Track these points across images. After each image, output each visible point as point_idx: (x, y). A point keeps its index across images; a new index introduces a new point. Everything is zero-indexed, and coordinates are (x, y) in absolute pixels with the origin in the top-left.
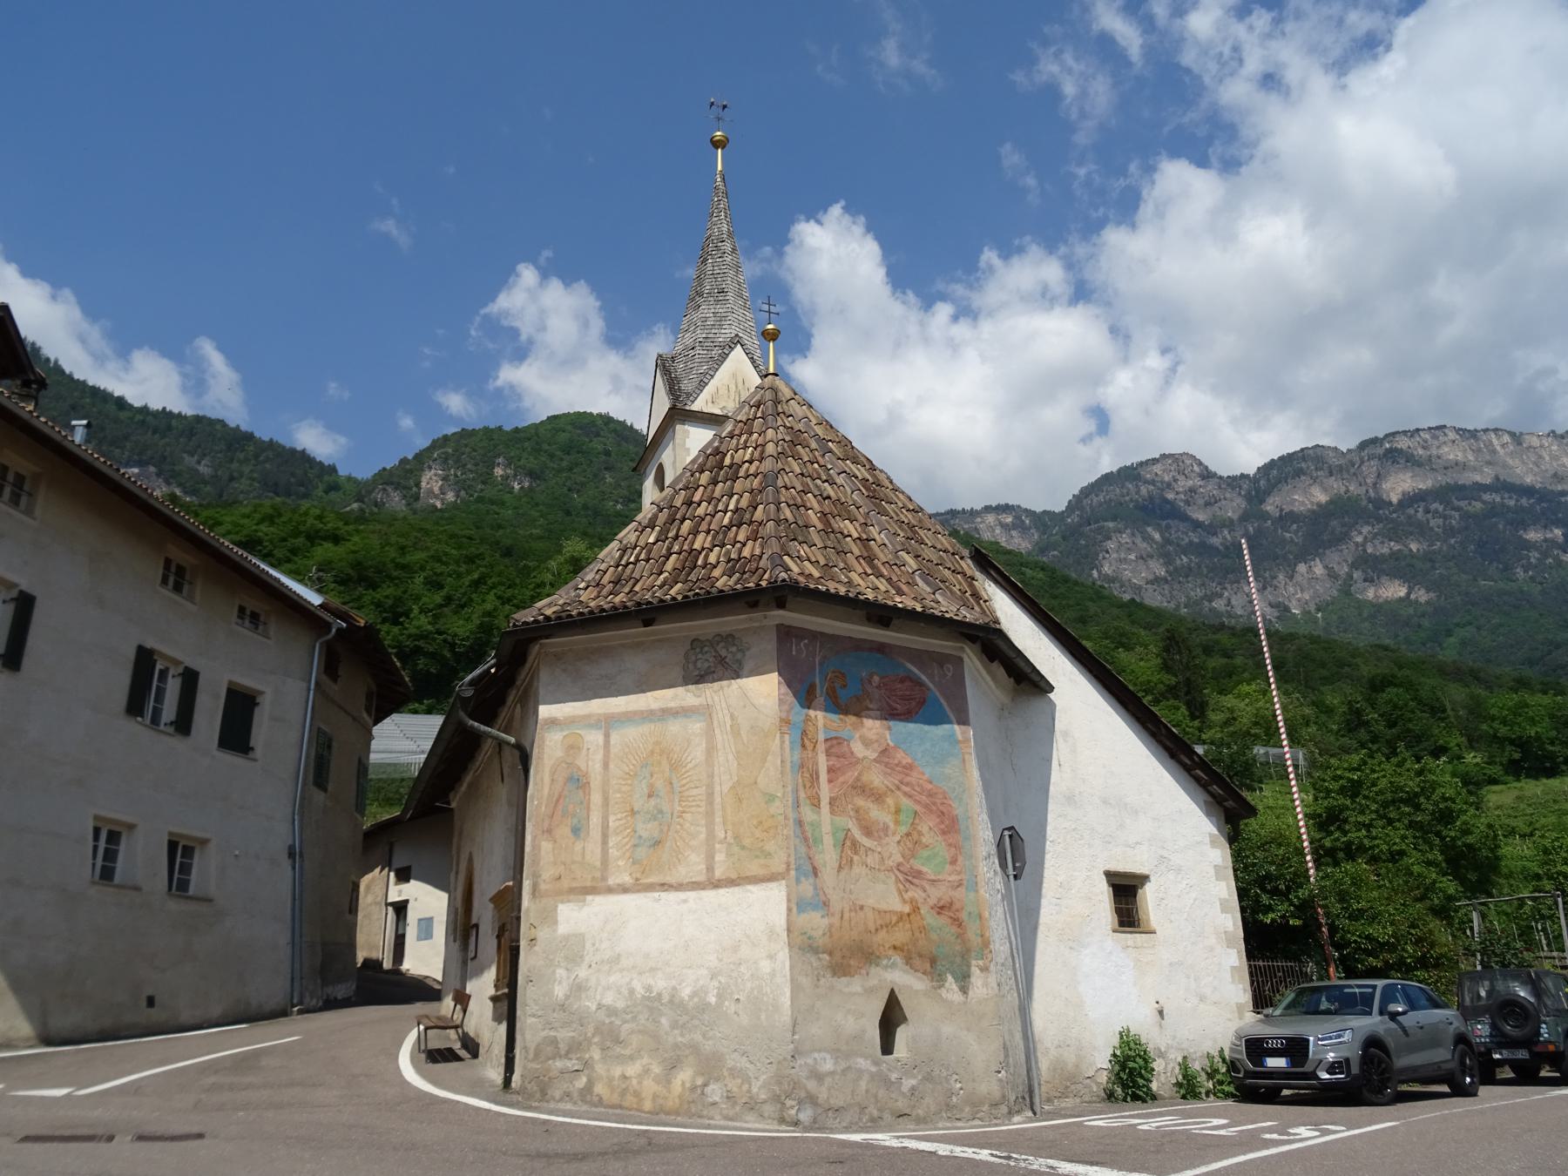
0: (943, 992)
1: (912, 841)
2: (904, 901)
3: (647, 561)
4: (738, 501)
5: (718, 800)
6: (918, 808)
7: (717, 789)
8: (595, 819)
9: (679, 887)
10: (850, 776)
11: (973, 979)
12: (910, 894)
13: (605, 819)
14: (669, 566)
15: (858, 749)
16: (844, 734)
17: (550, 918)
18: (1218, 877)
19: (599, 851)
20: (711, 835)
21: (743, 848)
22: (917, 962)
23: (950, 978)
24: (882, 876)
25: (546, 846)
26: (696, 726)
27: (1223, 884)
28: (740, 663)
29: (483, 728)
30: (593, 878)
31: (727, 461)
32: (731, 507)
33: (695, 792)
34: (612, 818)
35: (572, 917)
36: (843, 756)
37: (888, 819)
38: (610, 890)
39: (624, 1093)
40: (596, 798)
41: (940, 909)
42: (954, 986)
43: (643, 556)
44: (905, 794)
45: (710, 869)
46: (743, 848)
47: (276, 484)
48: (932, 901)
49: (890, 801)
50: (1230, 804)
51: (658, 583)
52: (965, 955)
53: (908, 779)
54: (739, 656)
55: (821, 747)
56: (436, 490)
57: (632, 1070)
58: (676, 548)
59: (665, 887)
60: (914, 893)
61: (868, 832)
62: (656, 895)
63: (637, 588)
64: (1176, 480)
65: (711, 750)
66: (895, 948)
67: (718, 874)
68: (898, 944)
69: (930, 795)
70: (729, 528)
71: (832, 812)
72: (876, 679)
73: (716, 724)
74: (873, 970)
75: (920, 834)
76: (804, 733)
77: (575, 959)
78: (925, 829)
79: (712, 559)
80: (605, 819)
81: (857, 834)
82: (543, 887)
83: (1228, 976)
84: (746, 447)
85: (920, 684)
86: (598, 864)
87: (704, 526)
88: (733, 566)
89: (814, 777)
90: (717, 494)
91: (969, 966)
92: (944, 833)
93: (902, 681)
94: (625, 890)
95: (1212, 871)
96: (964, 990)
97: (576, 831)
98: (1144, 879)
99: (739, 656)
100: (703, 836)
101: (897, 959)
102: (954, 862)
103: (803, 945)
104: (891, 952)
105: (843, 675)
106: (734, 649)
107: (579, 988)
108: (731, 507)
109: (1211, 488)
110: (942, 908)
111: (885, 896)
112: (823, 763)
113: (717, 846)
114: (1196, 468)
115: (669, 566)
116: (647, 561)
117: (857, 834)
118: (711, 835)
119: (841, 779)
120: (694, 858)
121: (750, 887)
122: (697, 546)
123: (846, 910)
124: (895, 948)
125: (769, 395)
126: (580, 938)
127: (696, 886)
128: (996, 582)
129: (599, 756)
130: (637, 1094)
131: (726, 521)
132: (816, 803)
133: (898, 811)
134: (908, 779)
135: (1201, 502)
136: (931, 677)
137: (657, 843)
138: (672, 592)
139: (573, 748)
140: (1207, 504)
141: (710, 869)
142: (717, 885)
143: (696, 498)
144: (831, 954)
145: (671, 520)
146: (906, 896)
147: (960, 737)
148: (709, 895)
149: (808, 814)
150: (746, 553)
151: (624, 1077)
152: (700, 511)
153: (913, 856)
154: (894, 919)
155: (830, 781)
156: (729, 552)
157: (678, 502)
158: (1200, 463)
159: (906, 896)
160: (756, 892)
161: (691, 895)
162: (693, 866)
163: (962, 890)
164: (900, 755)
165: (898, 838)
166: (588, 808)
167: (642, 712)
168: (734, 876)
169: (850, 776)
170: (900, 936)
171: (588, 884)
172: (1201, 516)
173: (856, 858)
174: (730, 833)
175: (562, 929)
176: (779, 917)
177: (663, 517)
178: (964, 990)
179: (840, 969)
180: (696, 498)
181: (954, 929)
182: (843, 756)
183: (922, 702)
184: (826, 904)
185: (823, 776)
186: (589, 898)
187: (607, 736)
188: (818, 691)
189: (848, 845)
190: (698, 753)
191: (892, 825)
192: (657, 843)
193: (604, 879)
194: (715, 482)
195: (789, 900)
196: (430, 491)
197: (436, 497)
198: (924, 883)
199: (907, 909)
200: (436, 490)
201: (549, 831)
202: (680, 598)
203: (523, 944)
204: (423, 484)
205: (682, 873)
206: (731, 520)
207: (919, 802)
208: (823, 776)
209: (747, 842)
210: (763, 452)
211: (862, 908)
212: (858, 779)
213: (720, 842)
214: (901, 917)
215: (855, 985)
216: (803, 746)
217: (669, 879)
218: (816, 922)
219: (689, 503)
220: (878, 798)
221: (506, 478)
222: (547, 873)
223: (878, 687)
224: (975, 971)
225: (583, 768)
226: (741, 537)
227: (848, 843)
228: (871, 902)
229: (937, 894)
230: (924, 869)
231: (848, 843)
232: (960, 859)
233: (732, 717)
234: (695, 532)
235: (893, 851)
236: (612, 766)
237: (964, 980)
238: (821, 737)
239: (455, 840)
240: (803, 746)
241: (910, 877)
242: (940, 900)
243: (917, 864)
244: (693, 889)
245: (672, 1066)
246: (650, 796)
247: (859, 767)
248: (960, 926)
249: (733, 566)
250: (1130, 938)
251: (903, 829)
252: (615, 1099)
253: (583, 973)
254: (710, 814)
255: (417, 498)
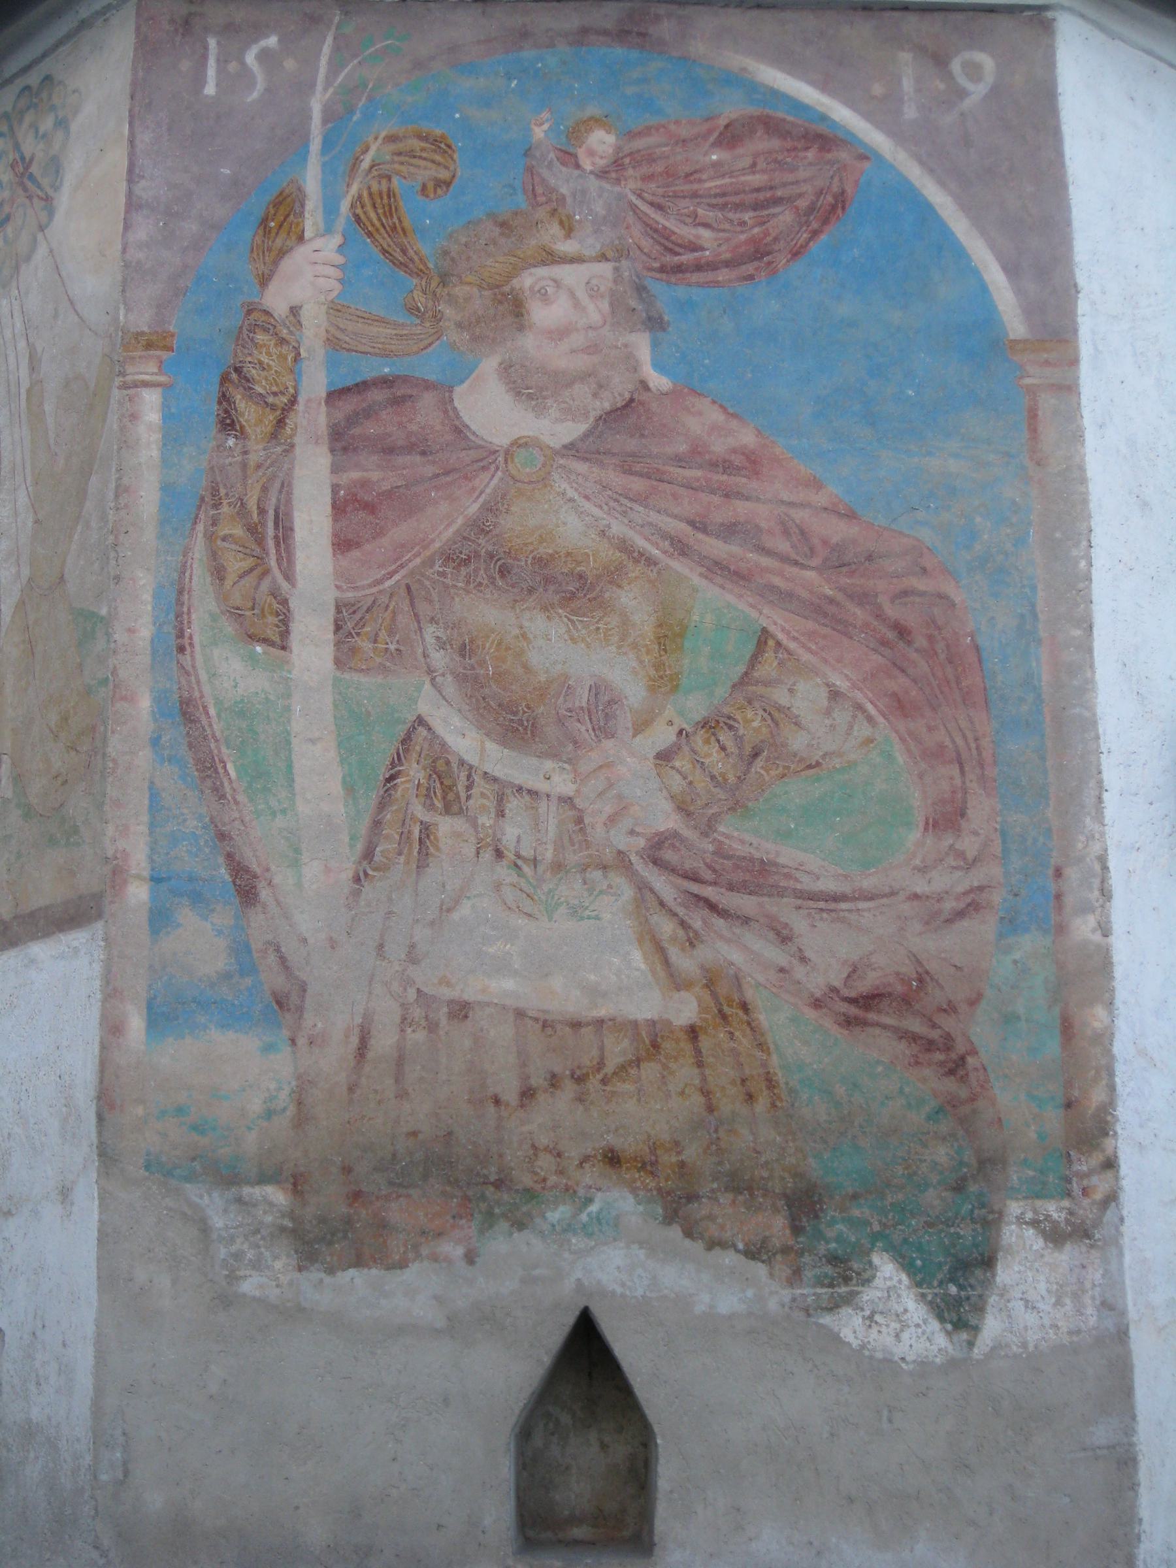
0: (849, 1326)
6: (775, 620)
10: (444, 521)
11: (1006, 1274)
12: (705, 953)
22: (722, 1211)
23: (886, 1270)
24: (571, 889)
36: (419, 447)
37: (628, 680)
41: (860, 1006)
42: (912, 1306)
44: (716, 568)
47: (127, 490)
48: (825, 972)
49: (633, 601)
52: (978, 1176)
55: (312, 419)
60: (741, 952)
61: (516, 724)
66: (613, 1159)
68: (628, 1144)
69: (838, 561)
71: (346, 655)
74: (500, 1244)
75: (776, 715)
76: (234, 377)
81: (463, 738)
85: (823, 139)
89: (270, 533)
92: (900, 706)
93: (730, 136)
96: (958, 1313)
102: (948, 817)
104: (589, 1176)
110: (869, 1001)
111: (600, 964)
112: (312, 481)
117: (463, 738)
119: (400, 532)
123: (387, 1012)
124: (613, 1159)
125: (573, 142)
133: (670, 635)
136: (883, 112)
144: (297, 1184)
147: (1016, 326)
149: (229, 672)
153: (737, 806)
154: (618, 1050)
155: (342, 544)
163: (984, 928)
164: (702, 421)
165: (662, 736)
170: (651, 1111)
173: (445, 826)
178: (958, 1313)
181: (930, 1083)
182: (419, 447)
185: (312, 523)
188: (311, 222)
199: (685, 1010)
207: (782, 597)
208: (312, 523)
211: (461, 1011)
212: (479, 527)
214: (652, 1042)
215: (411, 1292)
216: (228, 423)
218: (247, 1075)
220: (573, 588)
227: (414, 771)
229: (830, 952)
230: (788, 855)
231: (414, 771)
232: (980, 809)
235: (633, 785)
238: (315, 382)
240: (228, 423)
243: (743, 836)
247: (490, 483)
248: (956, 1068)
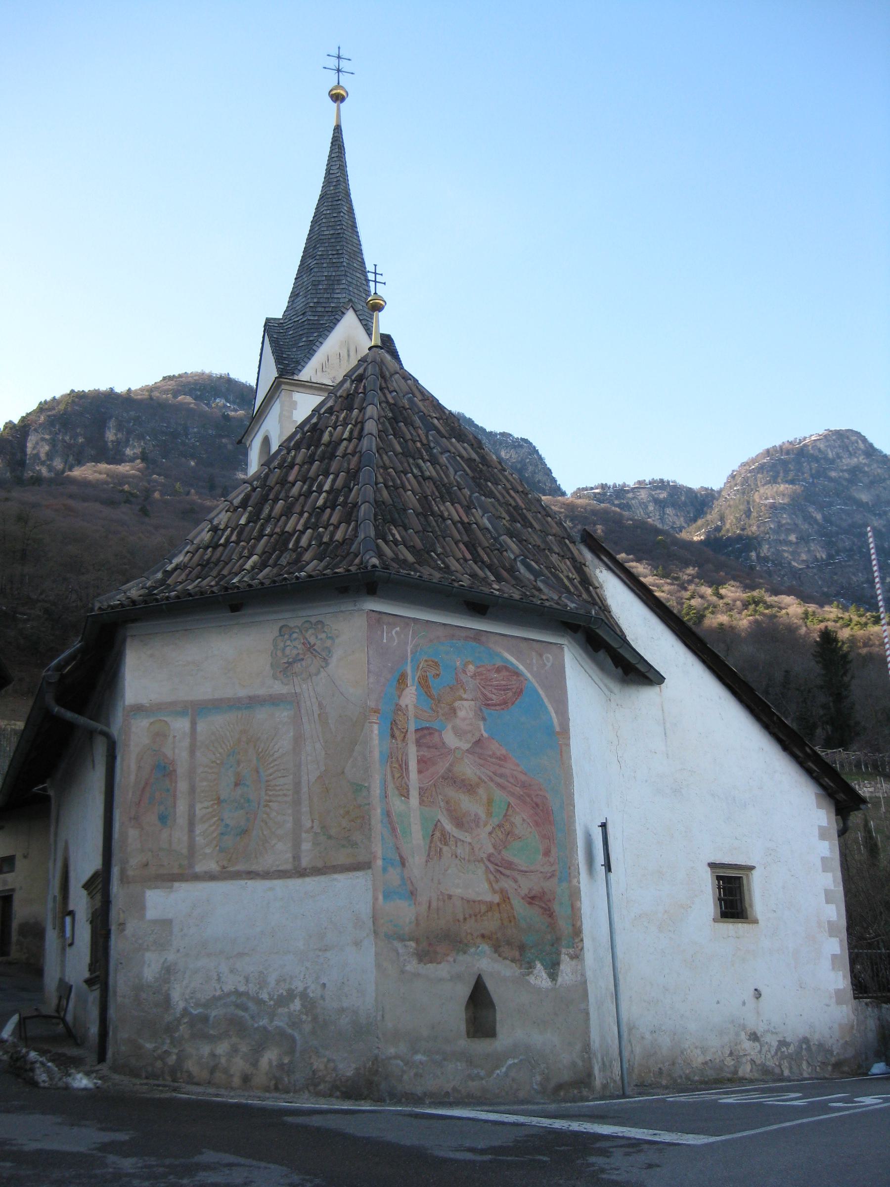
0: (532, 979)
1: (506, 834)
2: (494, 892)
3: (237, 543)
4: (334, 481)
5: (305, 789)
6: (512, 800)
7: (304, 779)
8: (182, 807)
9: (267, 875)
10: (441, 767)
11: (562, 967)
13: (192, 807)
14: (260, 548)
15: (450, 739)
16: (436, 725)
17: (140, 906)
18: (825, 869)
19: (185, 838)
20: (297, 823)
21: (330, 837)
23: (539, 966)
25: (133, 833)
26: (284, 714)
27: (830, 875)
28: (329, 650)
29: (69, 715)
30: (180, 866)
31: (326, 438)
32: (326, 487)
33: (281, 781)
34: (198, 806)
35: (159, 902)
36: (435, 747)
37: (481, 812)
38: (197, 878)
39: (213, 1071)
40: (182, 786)
41: (532, 899)
42: (545, 975)
43: (234, 538)
45: (296, 858)
46: (330, 837)
48: (524, 891)
49: (481, 791)
50: (841, 796)
51: (248, 566)
52: (556, 942)
53: (503, 770)
54: (328, 643)
55: (411, 737)
56: (43, 456)
57: (222, 1048)
58: (268, 530)
59: (252, 875)
60: (506, 884)
61: (459, 823)
62: (243, 882)
63: (225, 572)
64: (839, 457)
65: (298, 740)
66: (483, 936)
67: (305, 862)
69: (524, 786)
70: (323, 509)
72: (471, 668)
73: (303, 711)
75: (512, 824)
76: (394, 723)
77: (162, 945)
78: (517, 820)
79: (304, 542)
80: (192, 807)
81: (448, 826)
82: (130, 873)
83: (826, 963)
84: (345, 425)
85: (517, 674)
86: (185, 851)
87: (297, 508)
88: (325, 550)
89: (403, 767)
90: (311, 474)
91: (559, 954)
93: (498, 670)
94: (211, 877)
95: (819, 864)
96: (553, 976)
97: (163, 818)
98: (752, 868)
99: (328, 643)
100: (289, 825)
101: (485, 947)
102: (547, 853)
103: (385, 933)
104: (479, 940)
105: (436, 664)
106: (323, 636)
107: (168, 971)
108: (326, 487)
109: (877, 470)
110: (533, 898)
111: (476, 886)
113: (304, 835)
114: (861, 446)
115: (260, 548)
116: (237, 543)
117: (448, 826)
118: (297, 823)
120: (280, 846)
121: (336, 876)
122: (288, 528)
124: (483, 936)
126: (166, 924)
127: (282, 874)
128: (609, 568)
129: (186, 743)
130: (226, 1071)
131: (320, 502)
132: (404, 793)
133: (490, 802)
134: (503, 770)
135: (866, 480)
136: (529, 667)
137: (244, 832)
138: (260, 576)
139: (159, 736)
140: (872, 483)
141: (296, 858)
142: (301, 873)
143: (291, 478)
144: (417, 941)
145: (264, 499)
146: (496, 887)
148: (295, 884)
149: (397, 804)
150: (339, 536)
151: (213, 1055)
152: (295, 491)
154: (483, 908)
155: (420, 772)
156: (321, 536)
157: (272, 481)
158: (864, 440)
159: (496, 887)
160: (342, 881)
161: (278, 883)
162: (279, 854)
165: (489, 828)
166: (175, 796)
167: (229, 699)
168: (320, 864)
169: (441, 767)
170: (490, 924)
171: (176, 871)
172: (864, 497)
174: (316, 823)
175: (151, 914)
176: (364, 908)
177: (255, 496)
178: (553, 976)
179: (426, 954)
180: (291, 478)
182: (435, 747)
183: (519, 693)
184: (413, 894)
186: (176, 885)
187: (194, 724)
189: (437, 839)
190: (285, 743)
191: (483, 816)
192: (244, 832)
193: (191, 866)
194: (311, 460)
195: (375, 890)
196: (37, 456)
197: (43, 463)
198: (515, 874)
199: (496, 899)
200: (43, 456)
201: (136, 818)
202: (267, 582)
203: (113, 927)
204: (29, 450)
205: (268, 862)
206: (325, 503)
207: (512, 794)
209: (333, 832)
210: (362, 429)
212: (449, 770)
213: (307, 832)
214: (490, 906)
215: (442, 970)
216: (393, 736)
217: (254, 868)
218: (405, 913)
219: (283, 482)
220: (469, 788)
221: (118, 442)
222: (134, 861)
223: (474, 676)
224: (564, 958)
225: (169, 754)
226: (334, 520)
227: (438, 834)
228: (459, 891)
229: (527, 885)
230: (516, 860)
231: (438, 834)
233: (320, 705)
234: (287, 512)
236: (198, 754)
237: (553, 968)
238: (412, 727)
239: (52, 829)
240: (393, 736)
241: (500, 867)
242: (530, 890)
243: (507, 855)
244: (280, 877)
245: (258, 1049)
246: (237, 785)
249: (325, 550)
250: (731, 928)
251: (495, 821)
252: (205, 1075)
253: (171, 957)
254: (297, 803)
255: (22, 464)
